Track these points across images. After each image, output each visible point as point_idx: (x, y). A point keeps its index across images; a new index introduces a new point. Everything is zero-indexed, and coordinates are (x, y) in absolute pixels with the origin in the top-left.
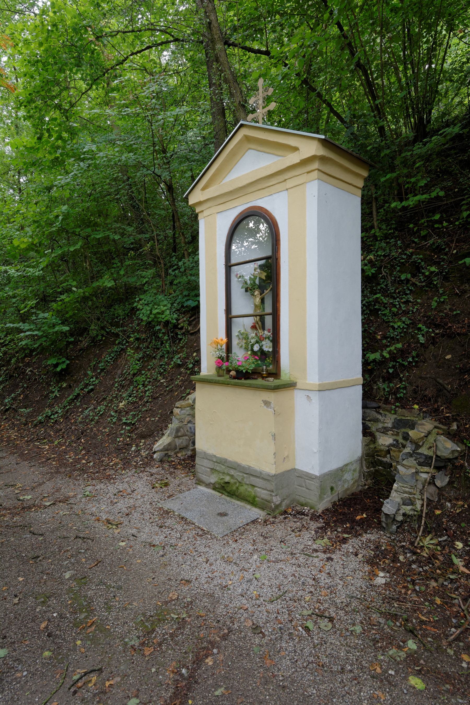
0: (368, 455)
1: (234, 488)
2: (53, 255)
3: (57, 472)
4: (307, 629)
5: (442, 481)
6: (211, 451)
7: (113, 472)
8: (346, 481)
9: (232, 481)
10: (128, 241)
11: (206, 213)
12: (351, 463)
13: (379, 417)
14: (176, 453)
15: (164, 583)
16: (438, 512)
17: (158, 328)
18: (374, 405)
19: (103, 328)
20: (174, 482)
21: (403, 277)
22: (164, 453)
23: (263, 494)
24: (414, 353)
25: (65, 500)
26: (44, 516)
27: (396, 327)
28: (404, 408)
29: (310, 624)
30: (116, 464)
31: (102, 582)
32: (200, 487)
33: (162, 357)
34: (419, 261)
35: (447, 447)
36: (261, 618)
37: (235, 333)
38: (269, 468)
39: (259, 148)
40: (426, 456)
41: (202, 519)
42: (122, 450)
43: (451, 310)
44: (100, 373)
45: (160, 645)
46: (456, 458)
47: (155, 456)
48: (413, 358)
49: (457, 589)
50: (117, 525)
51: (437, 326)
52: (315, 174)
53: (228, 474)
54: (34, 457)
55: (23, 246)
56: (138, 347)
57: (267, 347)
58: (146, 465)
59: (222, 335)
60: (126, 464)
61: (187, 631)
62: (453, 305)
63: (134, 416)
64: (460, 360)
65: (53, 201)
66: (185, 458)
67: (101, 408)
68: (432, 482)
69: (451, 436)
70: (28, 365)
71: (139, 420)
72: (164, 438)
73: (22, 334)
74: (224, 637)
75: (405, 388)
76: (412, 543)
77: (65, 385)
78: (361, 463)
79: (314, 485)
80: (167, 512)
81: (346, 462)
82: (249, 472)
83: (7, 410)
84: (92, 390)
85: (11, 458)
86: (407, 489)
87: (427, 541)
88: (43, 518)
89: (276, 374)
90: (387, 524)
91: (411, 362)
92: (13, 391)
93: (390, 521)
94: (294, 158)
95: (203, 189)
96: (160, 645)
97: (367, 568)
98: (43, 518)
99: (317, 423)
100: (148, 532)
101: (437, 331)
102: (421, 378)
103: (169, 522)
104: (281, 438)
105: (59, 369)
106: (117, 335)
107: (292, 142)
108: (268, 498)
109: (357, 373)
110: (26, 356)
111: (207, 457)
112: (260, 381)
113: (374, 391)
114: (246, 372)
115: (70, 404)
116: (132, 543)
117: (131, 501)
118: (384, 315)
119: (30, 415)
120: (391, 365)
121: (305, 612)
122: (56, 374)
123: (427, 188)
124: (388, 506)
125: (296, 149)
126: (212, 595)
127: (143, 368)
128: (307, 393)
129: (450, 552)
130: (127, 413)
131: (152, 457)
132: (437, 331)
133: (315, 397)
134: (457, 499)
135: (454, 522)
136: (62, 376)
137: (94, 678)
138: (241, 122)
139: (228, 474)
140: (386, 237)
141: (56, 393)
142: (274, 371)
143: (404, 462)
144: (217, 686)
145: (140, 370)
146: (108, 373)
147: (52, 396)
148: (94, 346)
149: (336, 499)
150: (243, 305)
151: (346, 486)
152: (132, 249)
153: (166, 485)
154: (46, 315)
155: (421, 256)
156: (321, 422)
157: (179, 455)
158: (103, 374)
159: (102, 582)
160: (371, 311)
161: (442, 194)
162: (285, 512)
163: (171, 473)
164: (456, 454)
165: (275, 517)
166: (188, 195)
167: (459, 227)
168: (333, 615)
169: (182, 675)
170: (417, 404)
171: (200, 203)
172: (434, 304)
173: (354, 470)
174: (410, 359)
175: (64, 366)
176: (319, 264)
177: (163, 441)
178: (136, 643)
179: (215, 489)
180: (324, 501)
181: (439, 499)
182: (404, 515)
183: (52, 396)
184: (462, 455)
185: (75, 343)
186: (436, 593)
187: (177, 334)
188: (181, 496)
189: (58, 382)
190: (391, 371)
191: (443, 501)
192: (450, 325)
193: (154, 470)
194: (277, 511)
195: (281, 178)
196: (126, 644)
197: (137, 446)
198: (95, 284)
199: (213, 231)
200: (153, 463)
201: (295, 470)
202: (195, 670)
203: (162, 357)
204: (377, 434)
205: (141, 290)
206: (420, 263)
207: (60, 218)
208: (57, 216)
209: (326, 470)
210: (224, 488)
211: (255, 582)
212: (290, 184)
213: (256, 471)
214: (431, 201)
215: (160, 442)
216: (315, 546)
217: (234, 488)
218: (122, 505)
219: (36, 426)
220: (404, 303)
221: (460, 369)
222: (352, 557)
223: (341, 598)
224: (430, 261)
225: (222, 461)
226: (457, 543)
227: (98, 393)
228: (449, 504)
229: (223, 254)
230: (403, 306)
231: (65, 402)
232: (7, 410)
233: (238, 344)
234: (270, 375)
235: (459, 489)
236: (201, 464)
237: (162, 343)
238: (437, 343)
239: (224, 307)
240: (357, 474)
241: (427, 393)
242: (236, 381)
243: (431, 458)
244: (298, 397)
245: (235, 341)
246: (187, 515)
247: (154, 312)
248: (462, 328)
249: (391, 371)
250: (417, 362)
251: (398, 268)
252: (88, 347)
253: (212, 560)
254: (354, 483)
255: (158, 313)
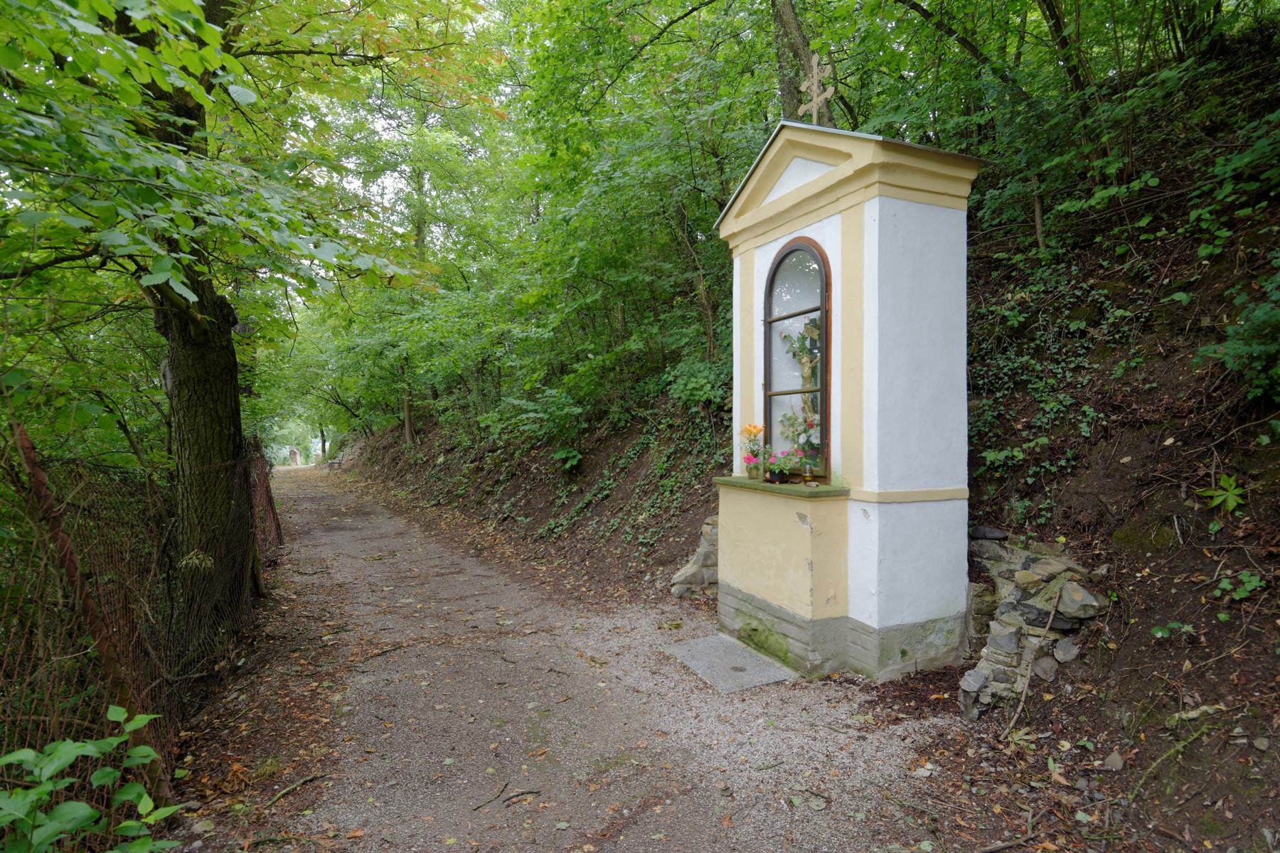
0: (978, 612)
1: (763, 638)
2: (567, 310)
3: (550, 599)
4: (790, 803)
5: (1067, 651)
6: (736, 584)
7: (615, 604)
8: (930, 645)
9: (760, 628)
10: (666, 284)
11: (741, 249)
12: (944, 620)
13: (1003, 553)
14: (703, 589)
15: (636, 731)
16: (1048, 697)
17: (694, 409)
18: (998, 534)
19: (628, 410)
20: (689, 624)
21: (1073, 327)
22: (685, 587)
23: (796, 647)
24: (1069, 454)
25: (550, 630)
26: (521, 643)
27: (1048, 409)
28: (1042, 541)
29: (797, 801)
30: (621, 596)
31: (565, 718)
32: (721, 634)
33: (701, 452)
34: (1103, 299)
35: (1076, 599)
36: (738, 782)
37: (777, 417)
38: (804, 611)
39: (806, 156)
40: (1040, 612)
41: (709, 671)
42: (633, 578)
43: (1145, 381)
44: (619, 474)
45: (609, 785)
46: (1092, 618)
47: (673, 590)
48: (1068, 460)
49: (1035, 801)
50: (601, 664)
51: (1117, 409)
52: (875, 189)
53: (756, 618)
54: (528, 579)
55: (532, 301)
56: (670, 438)
57: (816, 440)
58: (659, 600)
59: (760, 422)
60: (634, 596)
61: (644, 778)
62: (1151, 373)
63: (654, 534)
64: (1144, 465)
65: (573, 235)
66: (704, 595)
67: (615, 522)
68: (1044, 652)
69: (1090, 584)
70: (534, 460)
71: (659, 540)
72: (689, 566)
73: (524, 416)
74: (684, 793)
75: (1050, 509)
76: (996, 737)
77: (575, 489)
78: (966, 623)
79: (872, 643)
80: (668, 658)
81: (933, 617)
82: (782, 616)
83: (505, 519)
84: (608, 496)
85: (501, 577)
86: (1001, 658)
87: (1020, 736)
88: (519, 646)
89: (823, 478)
90: (966, 706)
91: (1065, 468)
92: (514, 494)
93: (970, 701)
94: (847, 169)
95: (737, 216)
96: (609, 785)
97: (912, 755)
98: (519, 646)
99: (876, 550)
100: (637, 676)
101: (1114, 418)
102: (1077, 493)
103: (665, 669)
104: (826, 564)
105: (567, 466)
106: (645, 421)
107: (843, 146)
108: (802, 653)
109: (958, 479)
110: (532, 448)
111: (732, 592)
112: (801, 487)
113: (1005, 513)
114: (781, 472)
115: (578, 514)
116: (613, 686)
117: (628, 640)
118: (1036, 390)
119: (530, 527)
120: (1031, 472)
121: (798, 787)
122: (564, 472)
123: (1124, 177)
124: (970, 679)
125: (848, 156)
126: (686, 751)
127: (674, 467)
128: (863, 506)
129: (1049, 754)
130: (646, 529)
131: (669, 591)
132: (1114, 418)
133: (874, 511)
134: (1084, 681)
135: (1069, 714)
136: (575, 473)
137: (530, 798)
138: (782, 122)
139: (756, 618)
140: (1057, 259)
141: (564, 499)
142: (822, 474)
143: (1004, 617)
144: (657, 831)
145: (668, 470)
146: (630, 473)
147: (559, 502)
148: (615, 435)
149: (912, 669)
150: (790, 376)
151: (932, 653)
152: (680, 294)
153: (678, 627)
154: (554, 392)
155: (1106, 291)
156: (882, 549)
157: (708, 592)
158: (623, 475)
159: (565, 718)
160: (1016, 384)
161: (1154, 182)
162: (829, 678)
163: (689, 614)
164: (1091, 612)
165: (811, 682)
166: (719, 225)
167: (1185, 238)
168: (834, 796)
169: (622, 815)
170: (1065, 535)
171: (734, 235)
172: (1118, 371)
173: (950, 632)
174: (1063, 463)
175: (575, 462)
176: (880, 316)
177: (688, 570)
178: (583, 778)
179: (739, 638)
180: (888, 669)
181: (1056, 680)
182: (993, 695)
183: (559, 502)
184: (1100, 614)
185: (591, 430)
186: (1001, 799)
187: (722, 419)
188: (692, 642)
189: (567, 484)
190: (1030, 481)
191: (1061, 683)
192: (1134, 406)
193: (668, 608)
194: (815, 675)
195: (832, 196)
196: (573, 777)
197: (653, 574)
198: (618, 349)
199: (750, 271)
200: (669, 599)
201: (847, 618)
202: (638, 813)
203: (701, 452)
204: (999, 581)
205: (675, 357)
206: (1103, 303)
207: (576, 260)
208: (572, 258)
209: (893, 622)
210: (751, 638)
211: (748, 747)
212: (843, 204)
213: (788, 614)
214: (1131, 196)
215: (682, 571)
216: (849, 722)
217: (763, 638)
218: (614, 644)
219: (536, 541)
220: (1073, 370)
221: (1139, 479)
222: (896, 741)
223: (854, 782)
224: (1120, 299)
225: (748, 599)
226: (1063, 742)
227: (615, 500)
228: (1069, 688)
229: (762, 306)
230: (1068, 374)
231: (573, 511)
232: (505, 519)
233: (782, 433)
234: (815, 478)
235: (1092, 668)
236: (726, 604)
237: (701, 433)
238: (1112, 436)
239: (762, 381)
240: (955, 640)
241: (1080, 517)
242: (768, 484)
243: (1048, 614)
244: (854, 511)
245: (777, 430)
246: (692, 665)
247: (690, 386)
248: (1154, 411)
249: (1030, 481)
250: (1074, 467)
251: (1067, 312)
252: (608, 438)
253: (703, 716)
254: (948, 652)
255: (694, 389)
